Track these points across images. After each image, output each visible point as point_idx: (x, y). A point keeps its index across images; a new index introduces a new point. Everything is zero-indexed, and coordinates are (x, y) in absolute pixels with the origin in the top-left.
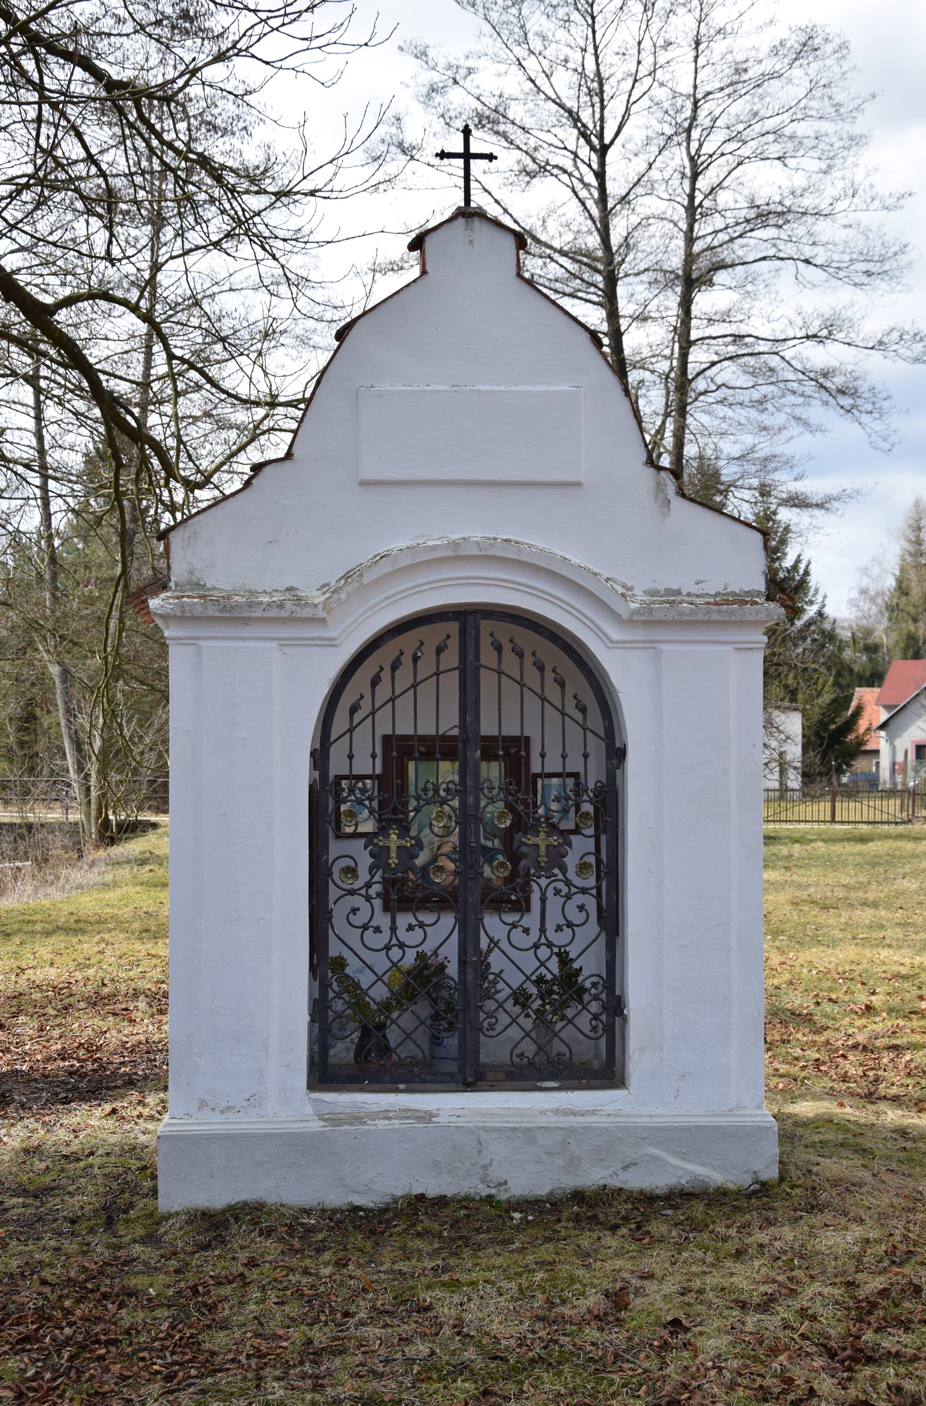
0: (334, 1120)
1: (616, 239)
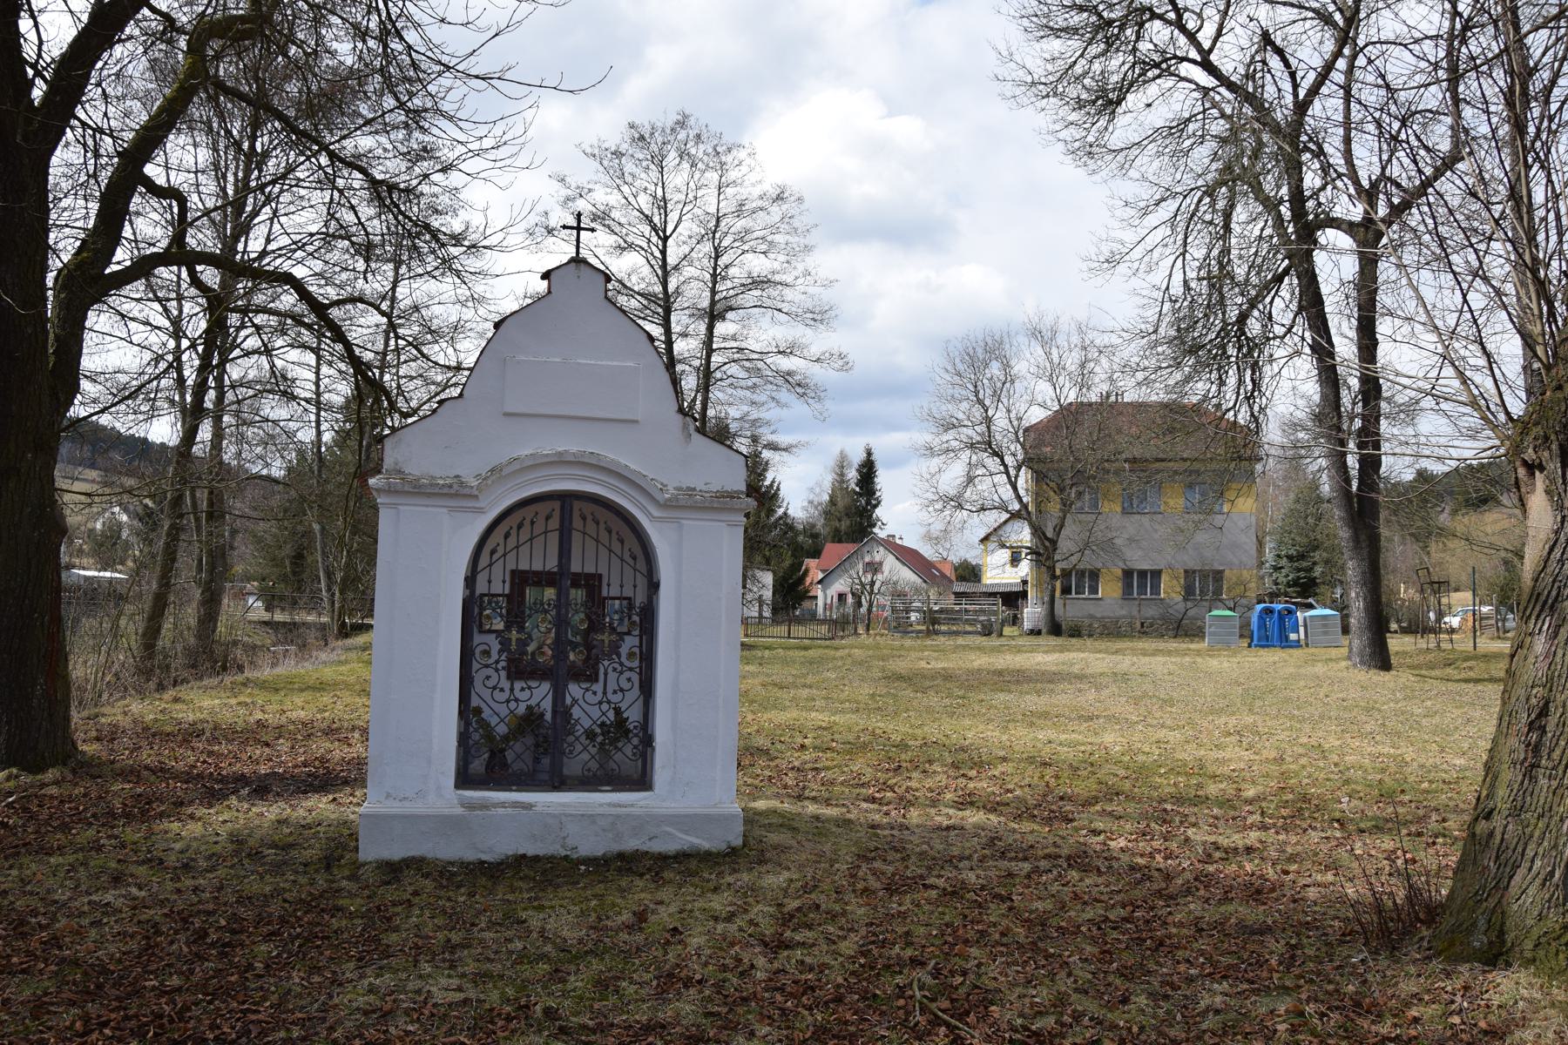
0: (470, 806)
1: (671, 288)
